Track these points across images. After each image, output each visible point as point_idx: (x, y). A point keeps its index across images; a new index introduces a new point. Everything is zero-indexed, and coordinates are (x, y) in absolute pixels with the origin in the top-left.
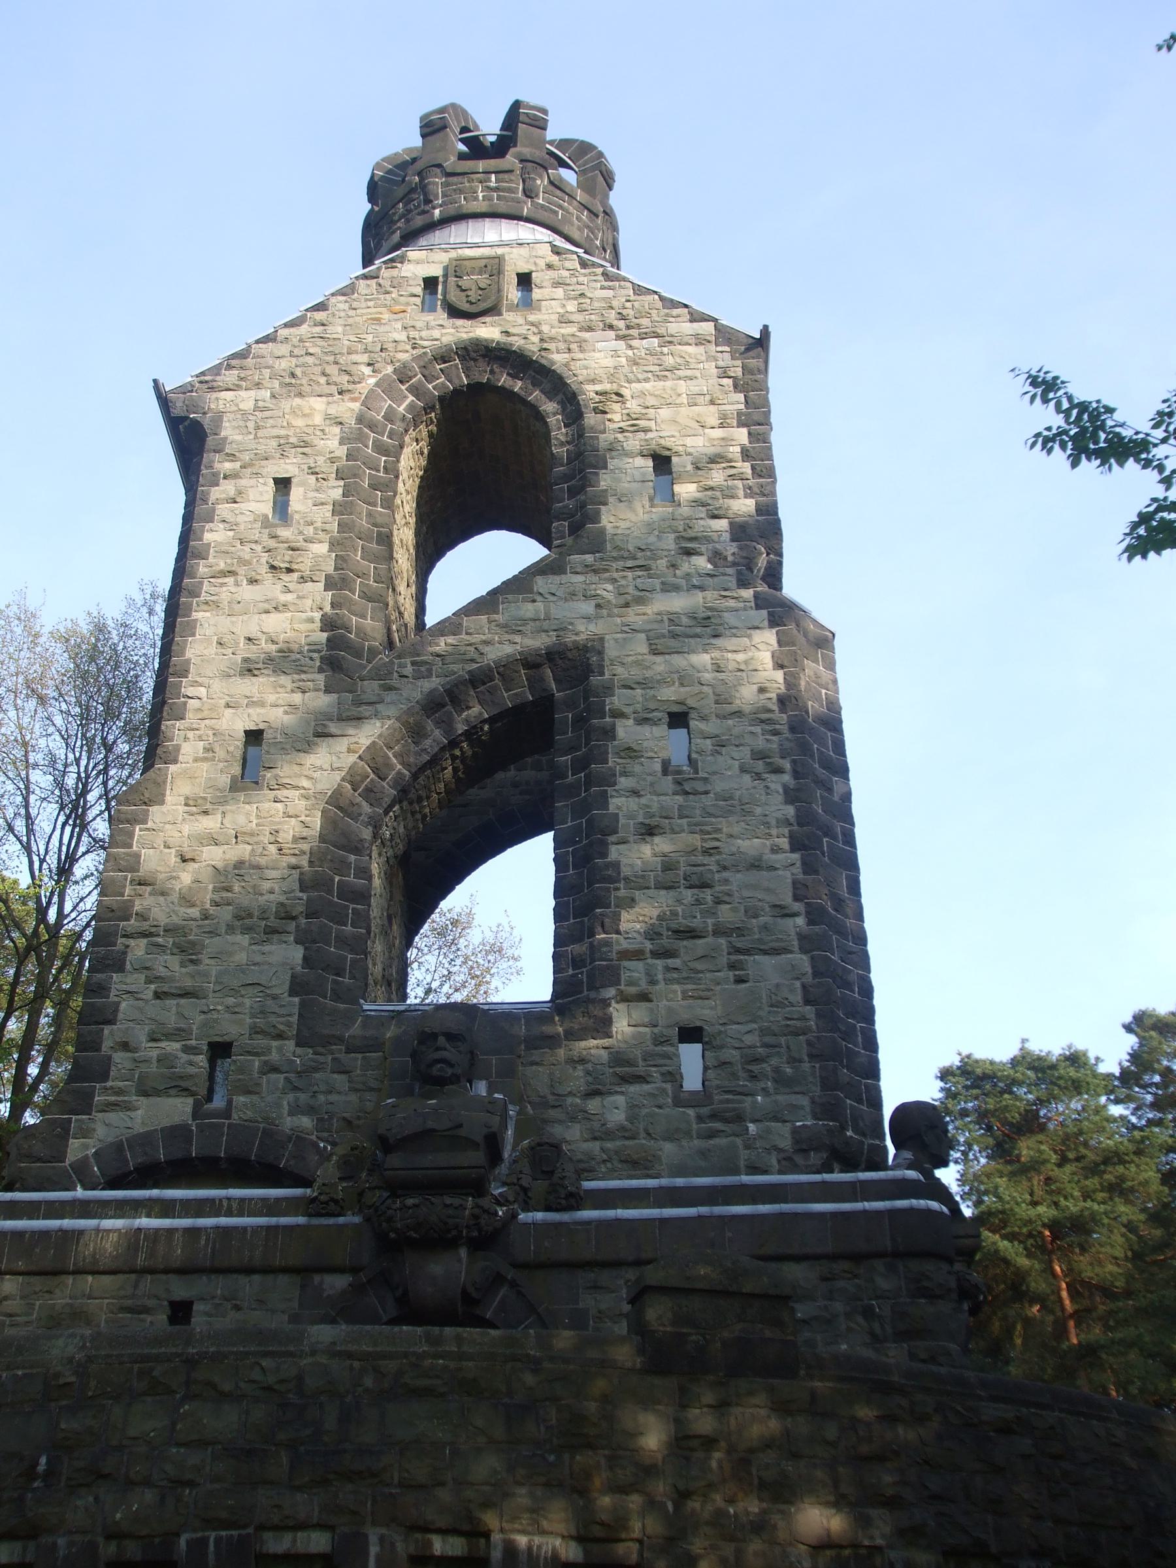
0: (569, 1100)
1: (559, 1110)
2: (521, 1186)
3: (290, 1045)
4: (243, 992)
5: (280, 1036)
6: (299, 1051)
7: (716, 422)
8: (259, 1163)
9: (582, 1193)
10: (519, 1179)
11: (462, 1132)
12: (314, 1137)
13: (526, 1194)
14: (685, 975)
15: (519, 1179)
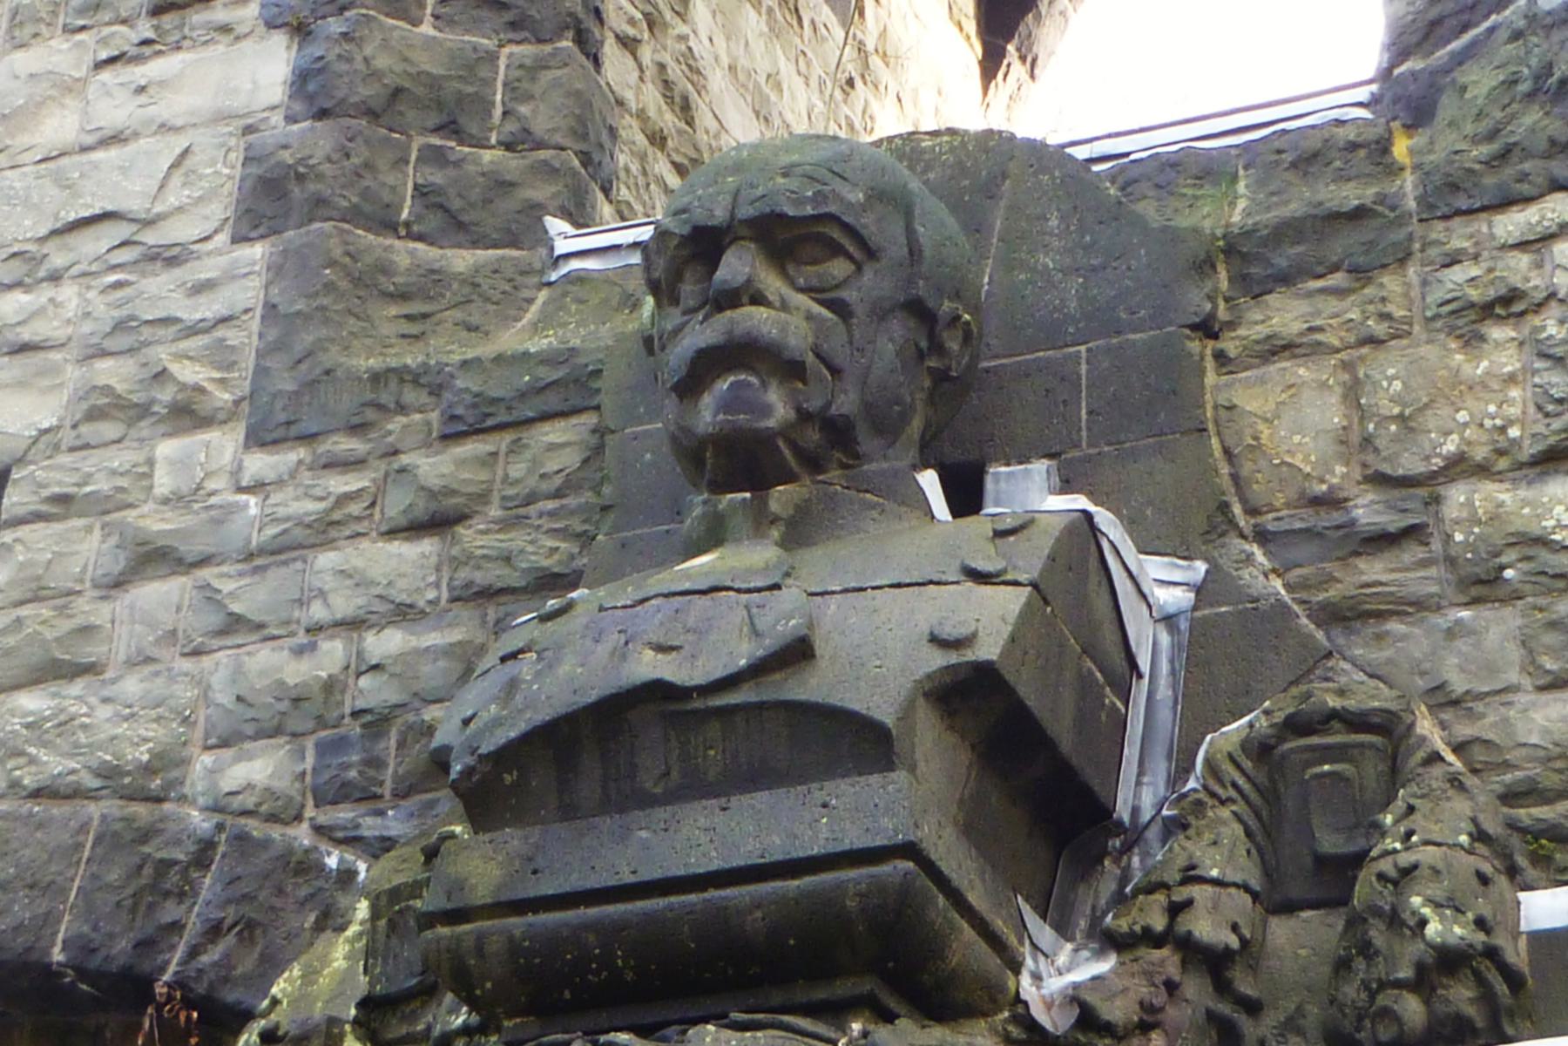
0: (1457, 496)
1: (1412, 553)
2: (1190, 949)
3: (224, 443)
4: (58, 260)
5: (188, 414)
6: (259, 464)
7: (310, 725)
8: (82, 973)
9: (1518, 955)
10: (1176, 910)
11: (810, 687)
12: (302, 835)
13: (1222, 987)
14: (532, 510)
15: (1176, 910)
